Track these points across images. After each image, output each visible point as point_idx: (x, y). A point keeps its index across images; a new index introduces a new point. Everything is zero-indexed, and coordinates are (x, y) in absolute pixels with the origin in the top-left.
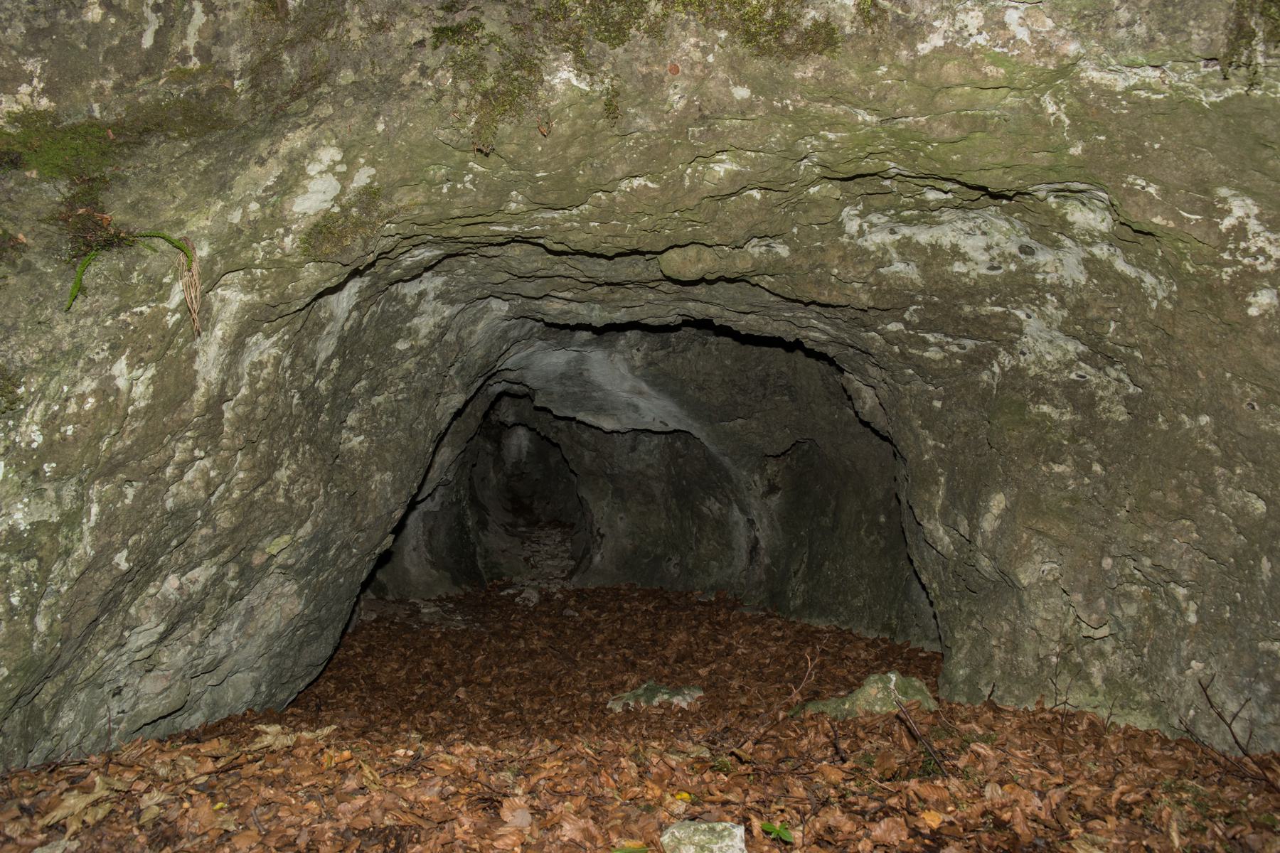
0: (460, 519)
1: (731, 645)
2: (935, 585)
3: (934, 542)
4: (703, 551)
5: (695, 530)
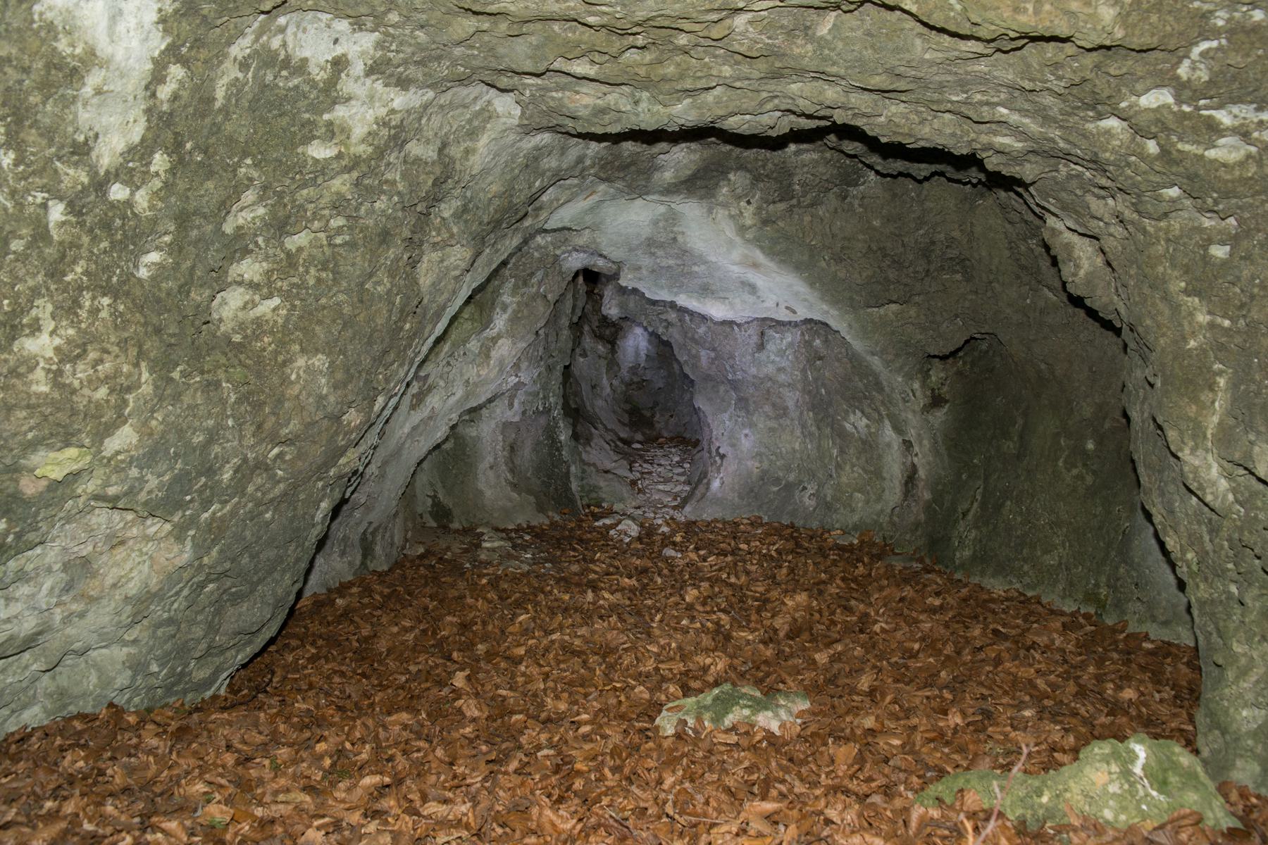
0: (550, 433)
1: (867, 615)
2: (1190, 556)
3: (1201, 487)
4: (844, 479)
5: (835, 452)
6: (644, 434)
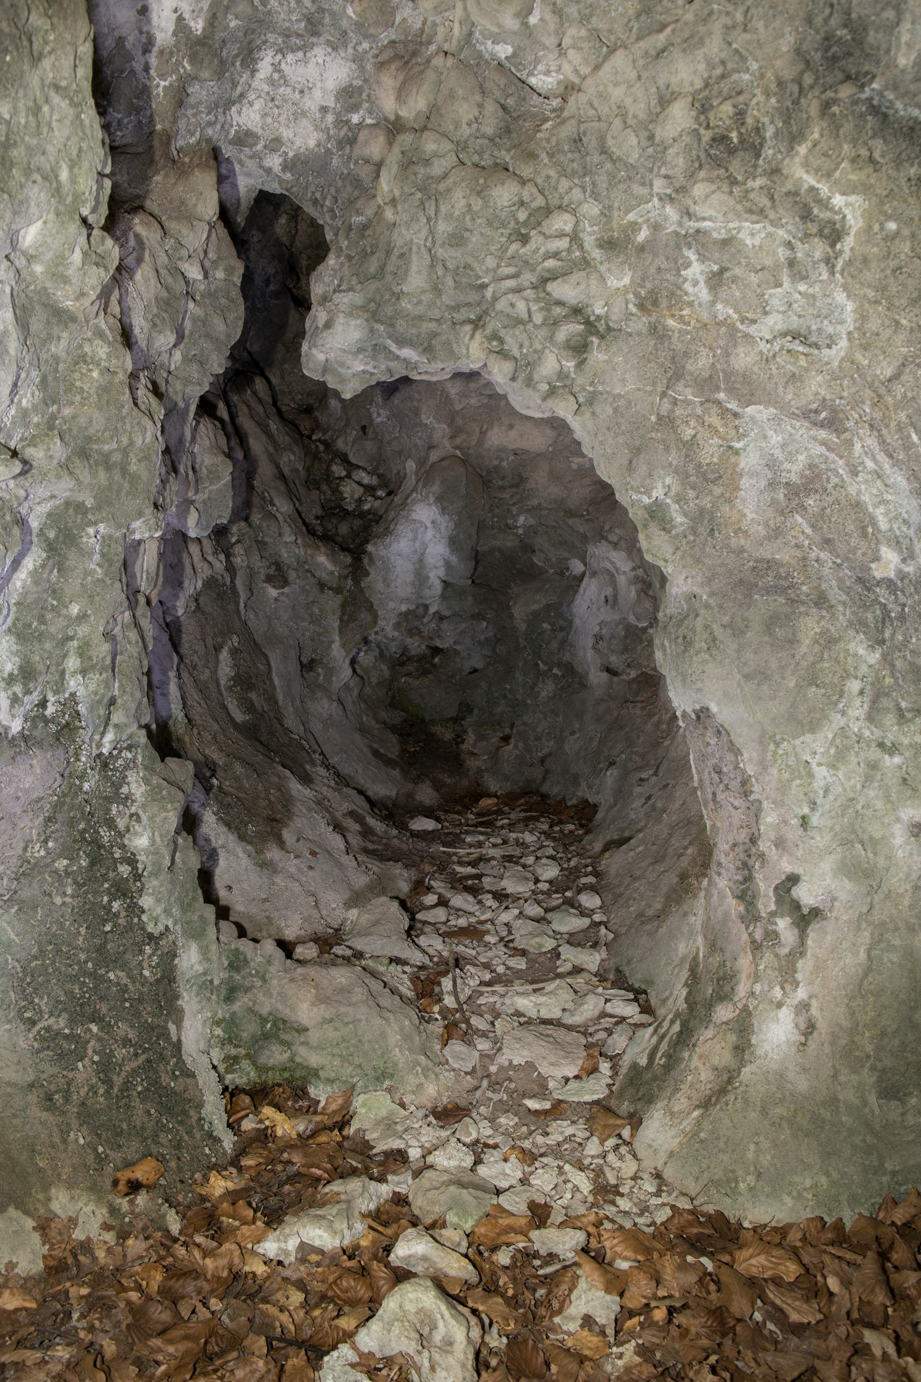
6: (438, 786)
